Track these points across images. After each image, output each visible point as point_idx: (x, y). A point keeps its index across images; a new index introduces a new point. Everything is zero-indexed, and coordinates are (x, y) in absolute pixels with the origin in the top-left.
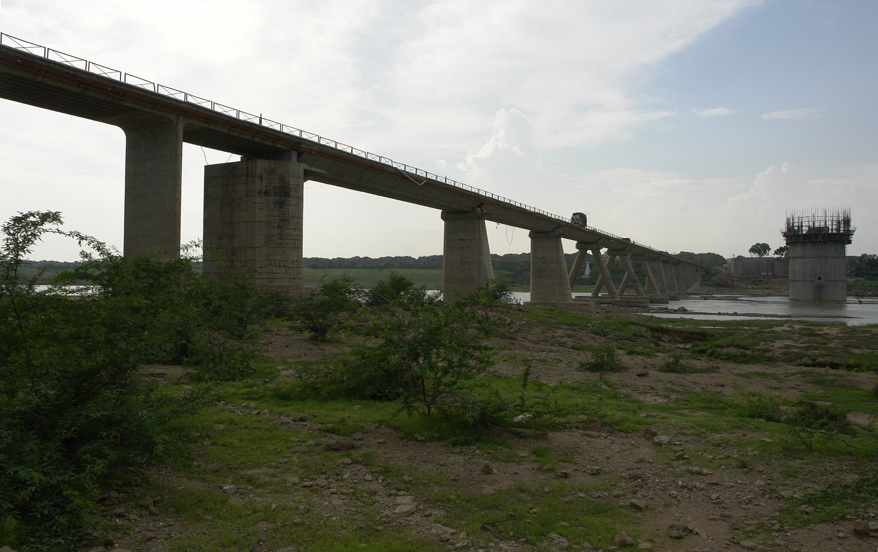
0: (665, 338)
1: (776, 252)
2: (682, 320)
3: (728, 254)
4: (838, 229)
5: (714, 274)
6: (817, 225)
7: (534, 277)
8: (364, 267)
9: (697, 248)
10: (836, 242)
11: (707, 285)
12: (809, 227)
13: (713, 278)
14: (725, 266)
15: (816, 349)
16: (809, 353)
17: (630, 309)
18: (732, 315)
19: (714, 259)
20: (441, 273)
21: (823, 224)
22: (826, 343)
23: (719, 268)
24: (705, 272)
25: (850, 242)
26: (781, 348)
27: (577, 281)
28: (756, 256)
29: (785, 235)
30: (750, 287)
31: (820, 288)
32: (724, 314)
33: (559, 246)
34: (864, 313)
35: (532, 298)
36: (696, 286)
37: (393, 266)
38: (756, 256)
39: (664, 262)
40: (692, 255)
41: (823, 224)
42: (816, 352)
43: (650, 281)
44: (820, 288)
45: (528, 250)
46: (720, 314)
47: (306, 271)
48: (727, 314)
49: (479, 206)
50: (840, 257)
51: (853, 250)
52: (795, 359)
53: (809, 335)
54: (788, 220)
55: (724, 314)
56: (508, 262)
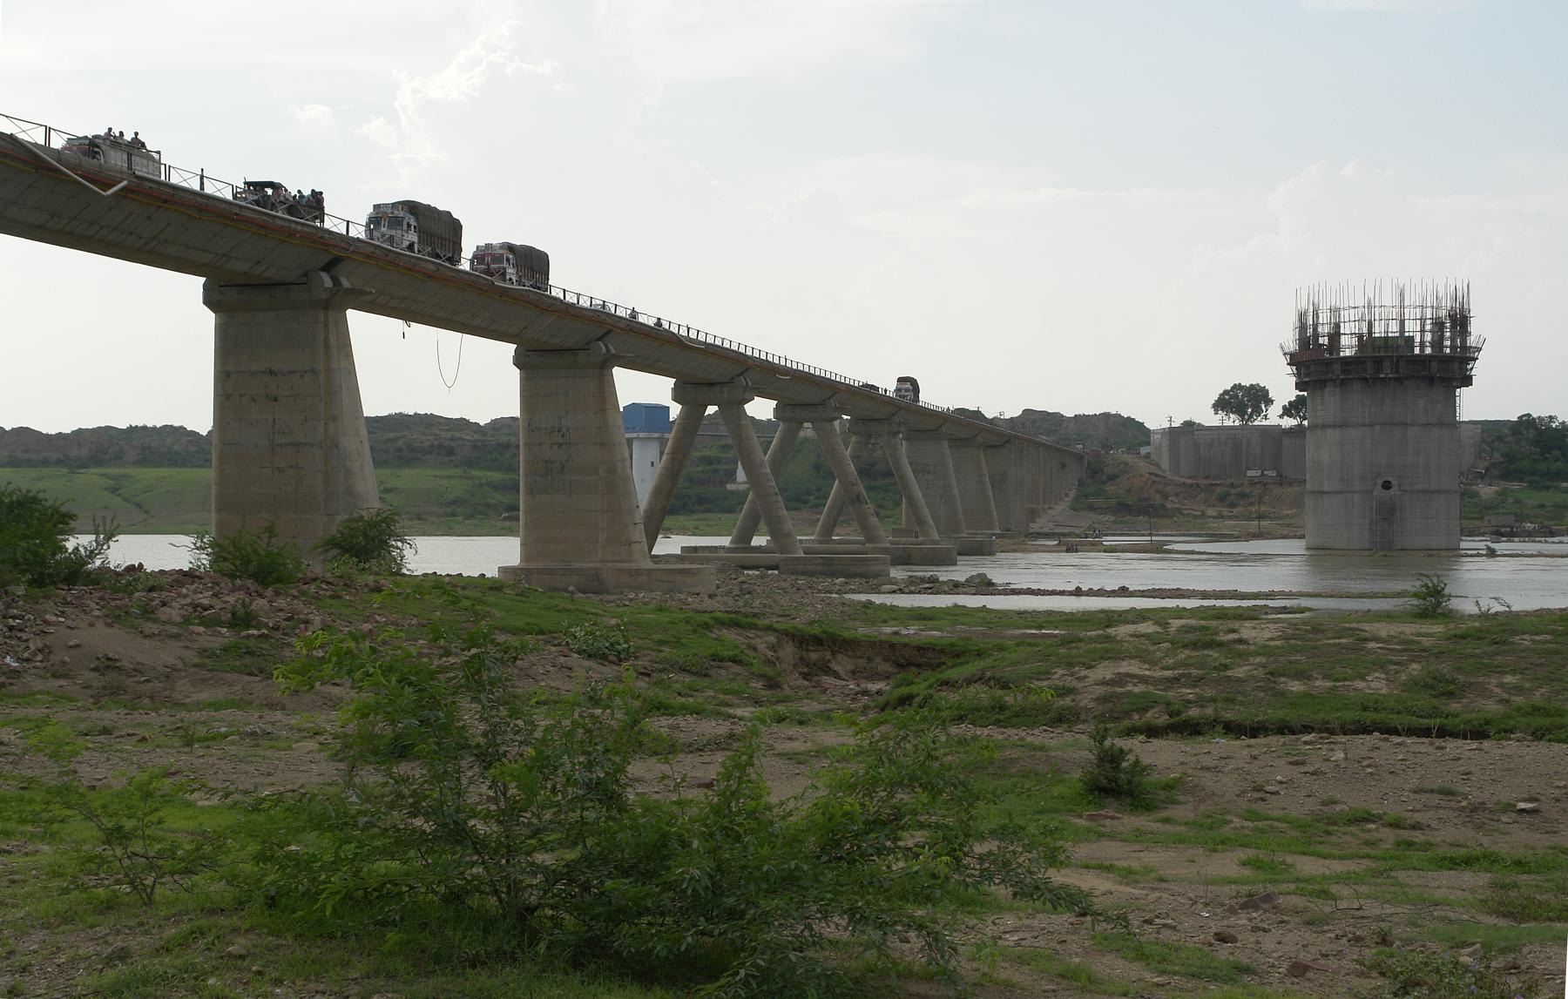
0: (842, 664)
1: (1288, 411)
2: (958, 612)
3: (1158, 410)
4: (1437, 343)
5: (1112, 478)
6: (1379, 331)
7: (531, 491)
9: (1073, 397)
10: (1431, 380)
11: (1092, 508)
12: (1360, 336)
13: (1110, 488)
14: (1144, 450)
15: (1197, 682)
16: (1171, 694)
17: (827, 582)
18: (1112, 594)
19: (1121, 431)
21: (1394, 328)
22: (1226, 667)
23: (1128, 458)
24: (1086, 471)
25: (1467, 381)
26: (1104, 683)
27: (676, 502)
28: (1232, 420)
29: (1294, 360)
30: (1211, 512)
31: (1387, 514)
32: (1091, 593)
33: (606, 391)
34: (1506, 580)
35: (526, 556)
36: (1058, 513)
37: (118, 458)
38: (1232, 420)
39: (958, 442)
40: (1054, 419)
41: (1394, 328)
42: (1189, 693)
43: (911, 501)
44: (1387, 514)
45: (511, 407)
46: (1078, 592)
48: (1101, 593)
49: (327, 268)
50: (1441, 425)
51: (1479, 403)
52: (1127, 714)
53: (1195, 645)
54: (1302, 316)
55: (1091, 593)
56: (420, 440)
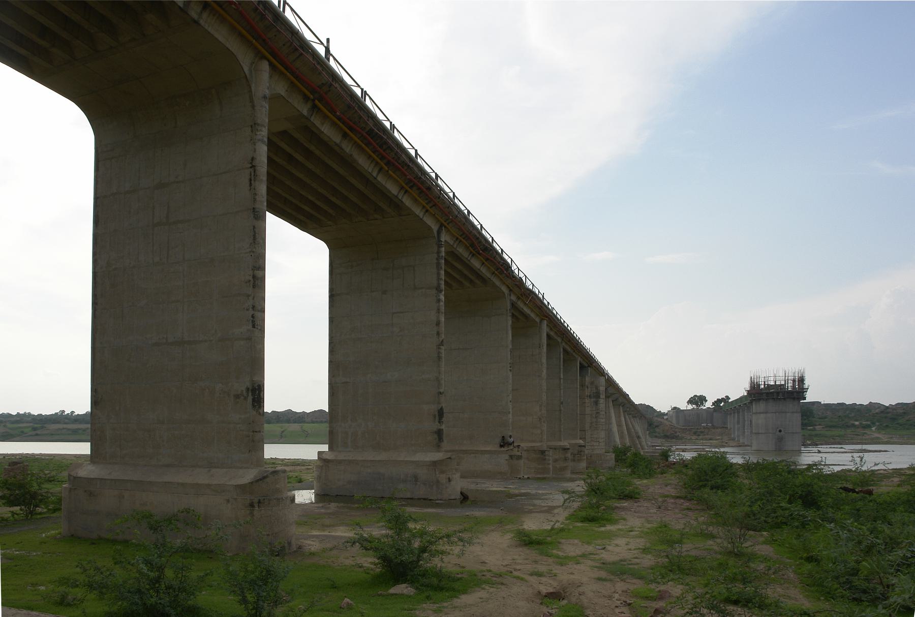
4: (794, 386)
5: (657, 426)
8: (313, 422)
10: (794, 399)
13: (657, 430)
20: (325, 427)
31: (780, 440)
44: (780, 440)
47: (89, 438)
